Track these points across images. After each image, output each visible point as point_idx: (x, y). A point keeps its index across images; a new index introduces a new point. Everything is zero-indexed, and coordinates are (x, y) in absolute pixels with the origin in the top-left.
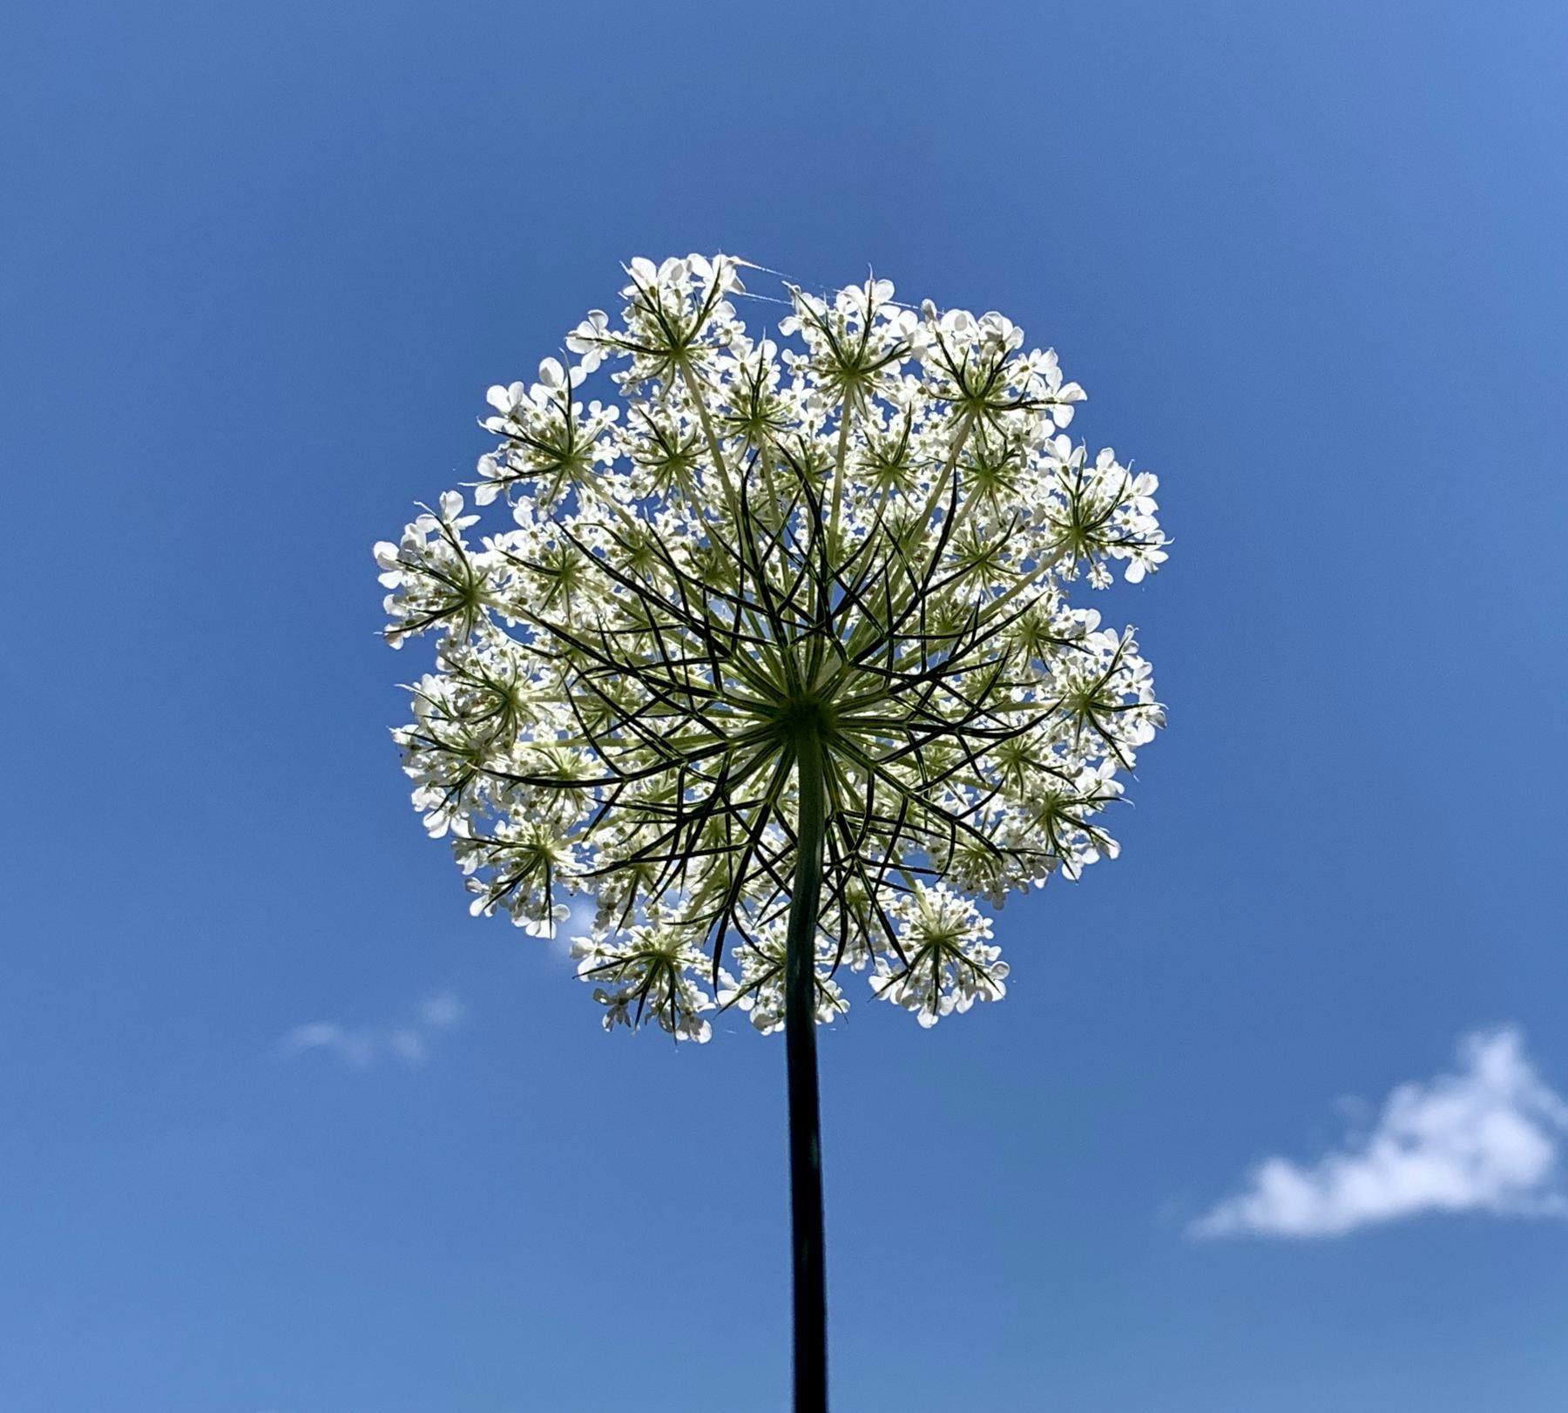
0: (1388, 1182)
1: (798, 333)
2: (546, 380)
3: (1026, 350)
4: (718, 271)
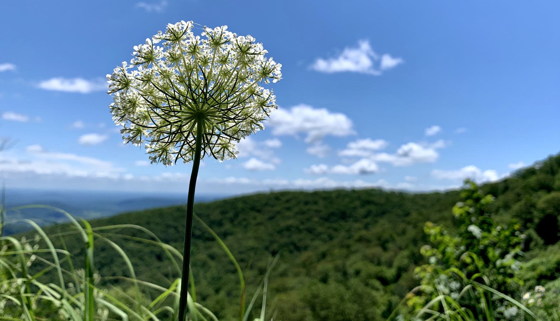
0: (342, 64)
1: (205, 36)
2: (147, 43)
3: (256, 42)
4: (190, 24)
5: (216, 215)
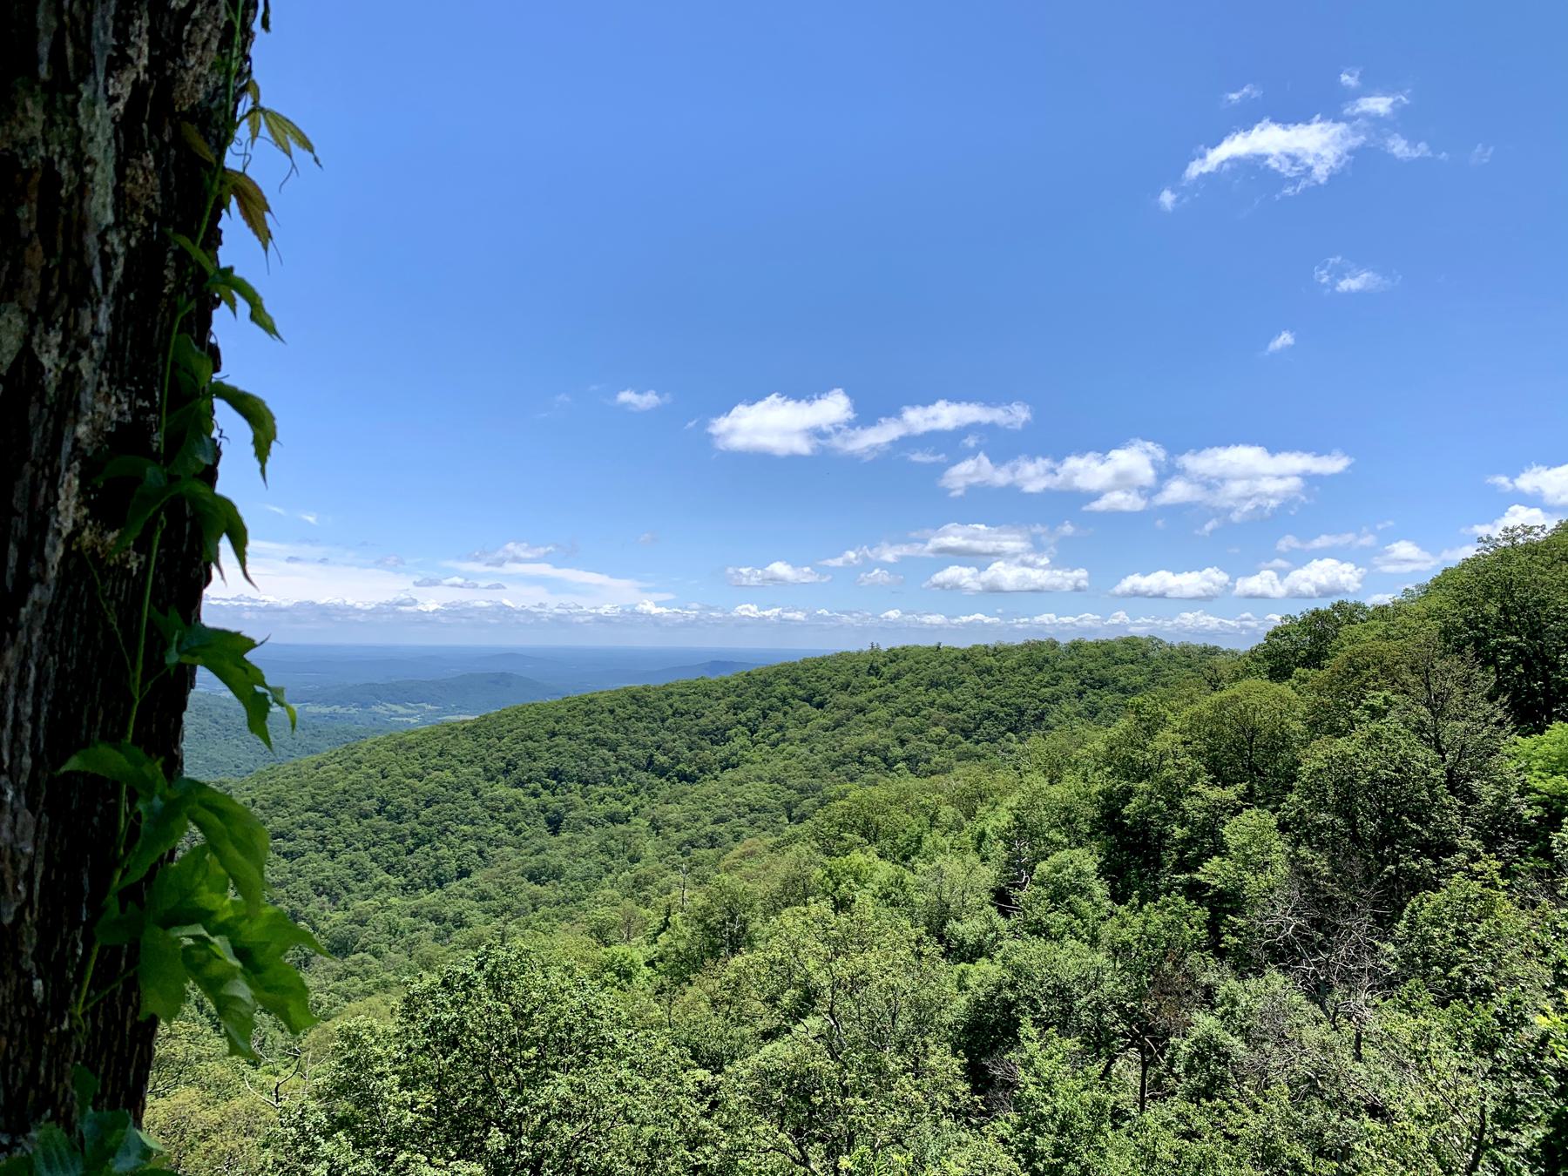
5: (717, 714)
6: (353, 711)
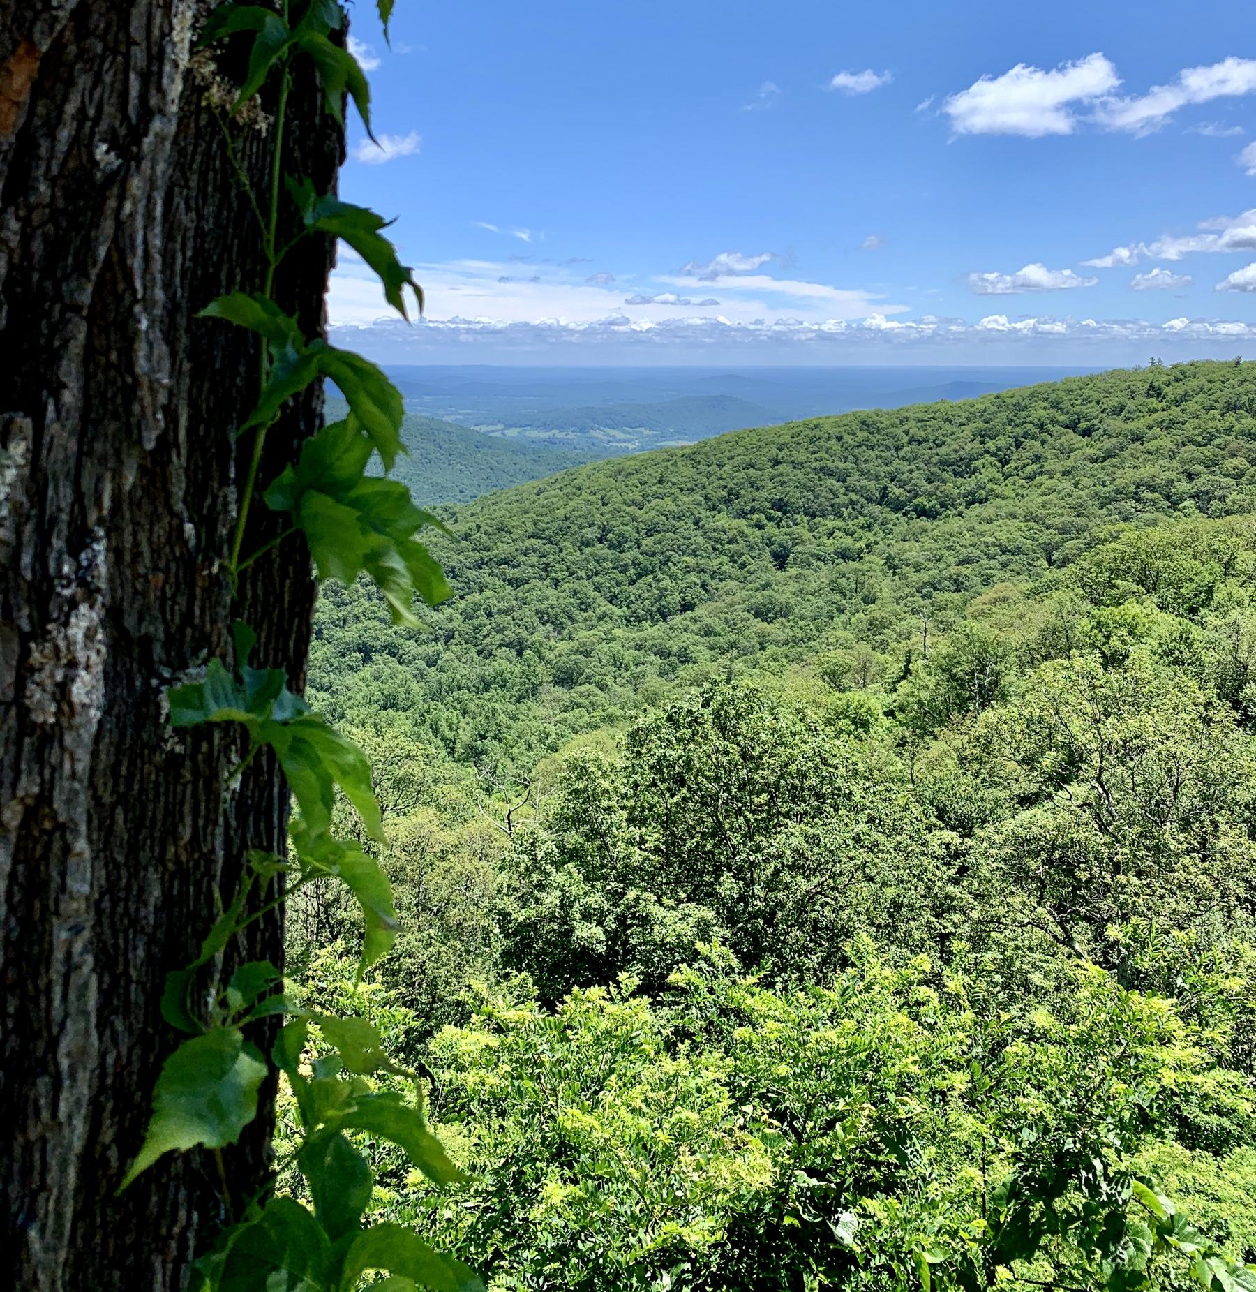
5: (961, 442)
6: (572, 435)
